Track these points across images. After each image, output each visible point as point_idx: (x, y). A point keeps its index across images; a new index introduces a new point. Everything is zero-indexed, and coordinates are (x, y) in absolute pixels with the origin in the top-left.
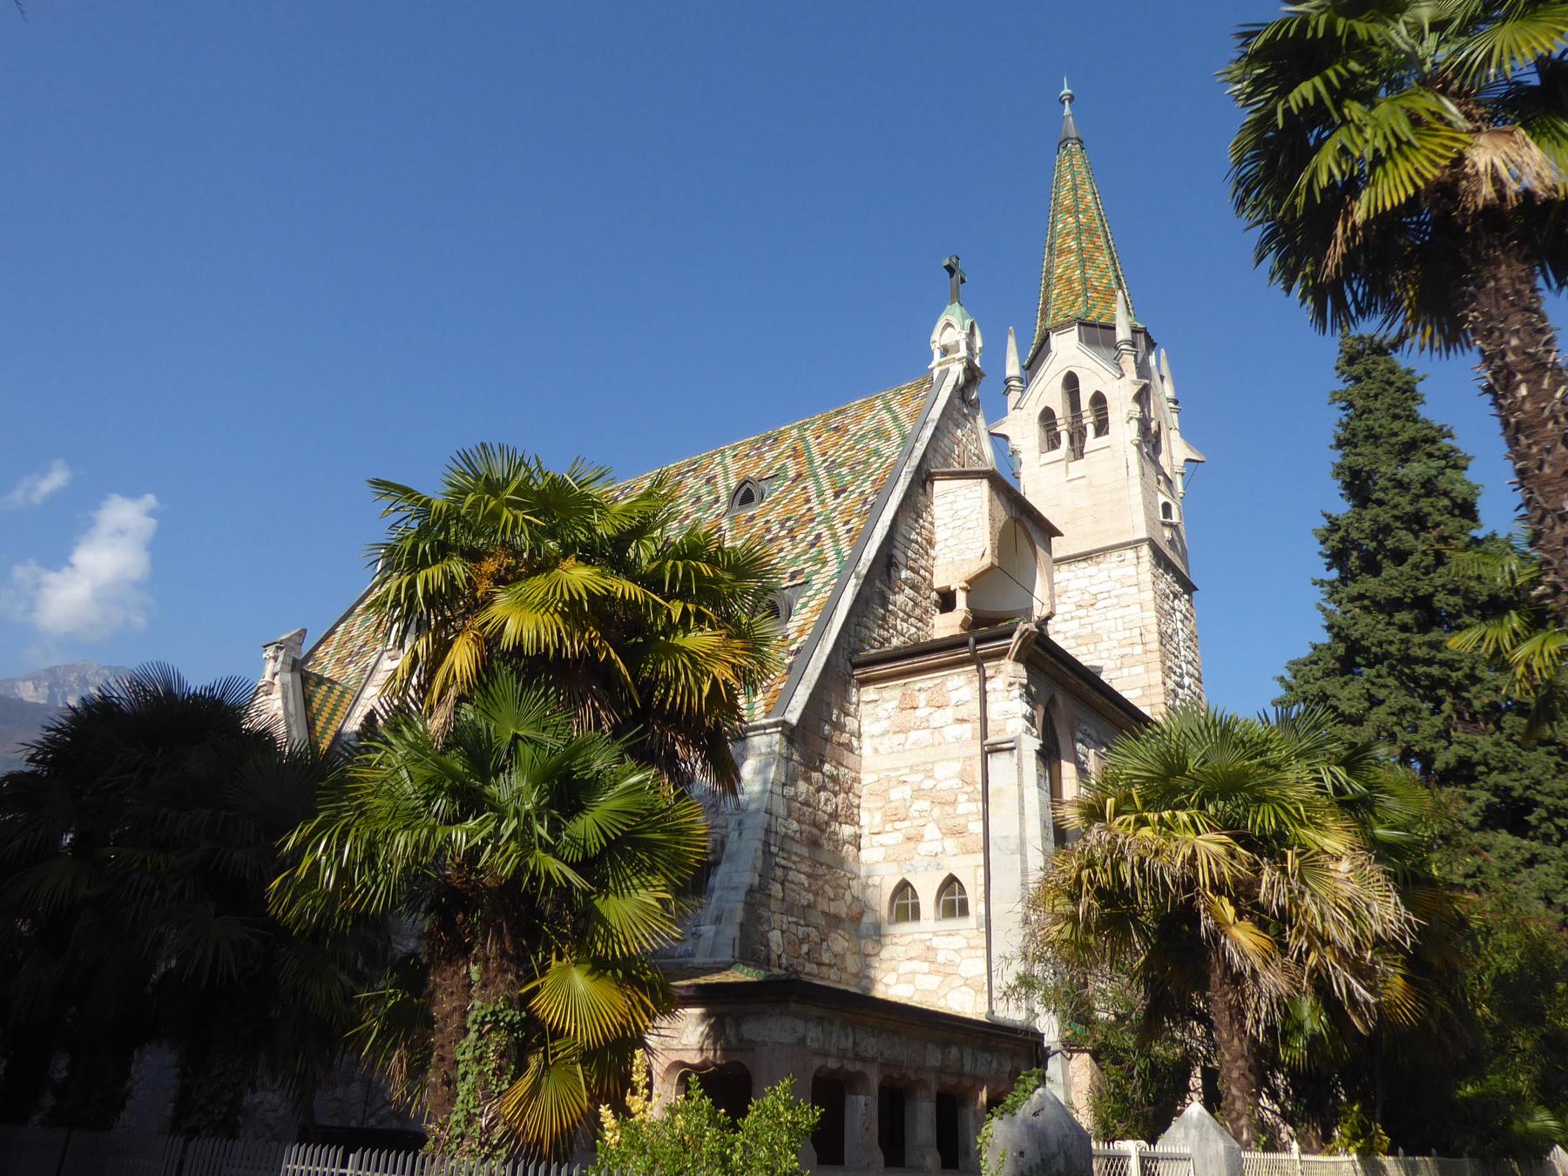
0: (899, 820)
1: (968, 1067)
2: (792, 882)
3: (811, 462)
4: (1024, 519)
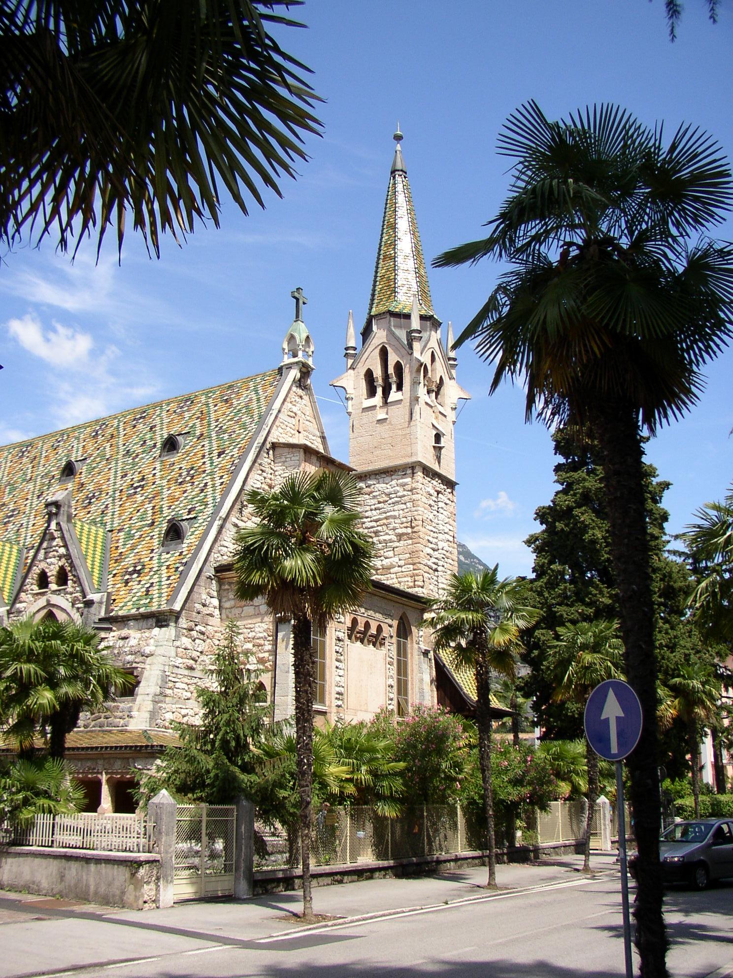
3: (209, 425)
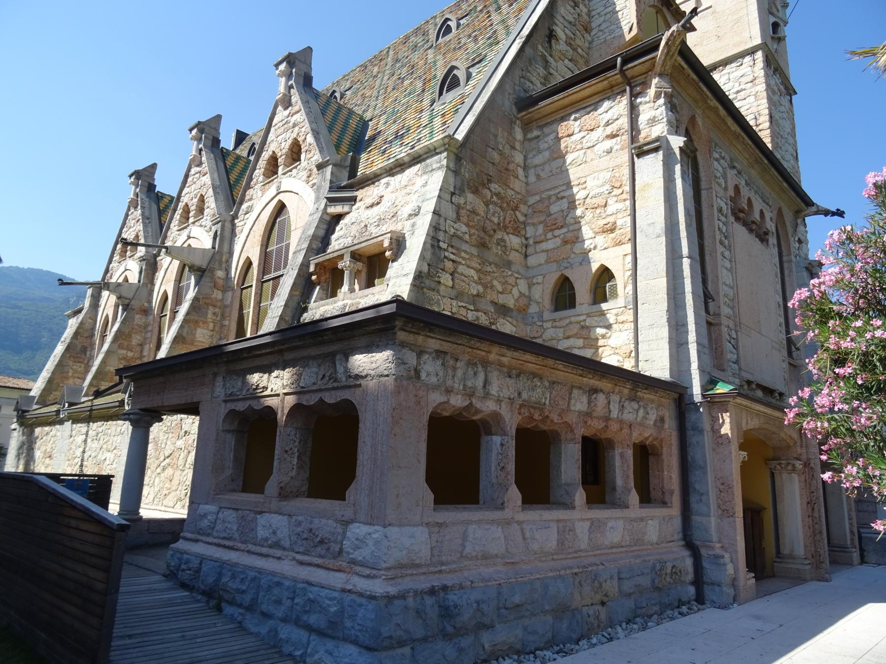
0: (557, 228)
1: (615, 414)
2: (462, 274)
4: (665, 10)
